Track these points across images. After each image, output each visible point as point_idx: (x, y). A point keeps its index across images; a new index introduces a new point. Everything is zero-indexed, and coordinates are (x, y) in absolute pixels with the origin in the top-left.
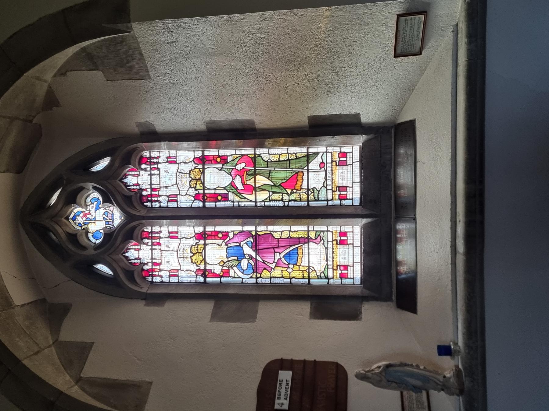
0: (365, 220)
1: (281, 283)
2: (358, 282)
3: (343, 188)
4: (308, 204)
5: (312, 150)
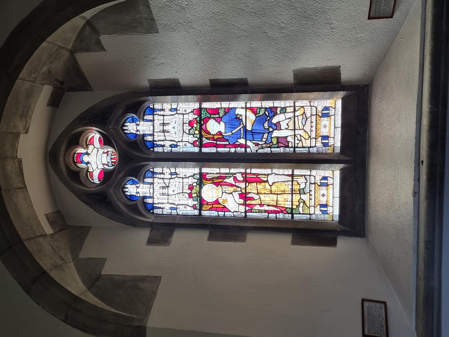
0: (342, 165)
1: (214, 216)
2: (336, 219)
3: (326, 137)
4: (294, 150)
5: (278, 104)
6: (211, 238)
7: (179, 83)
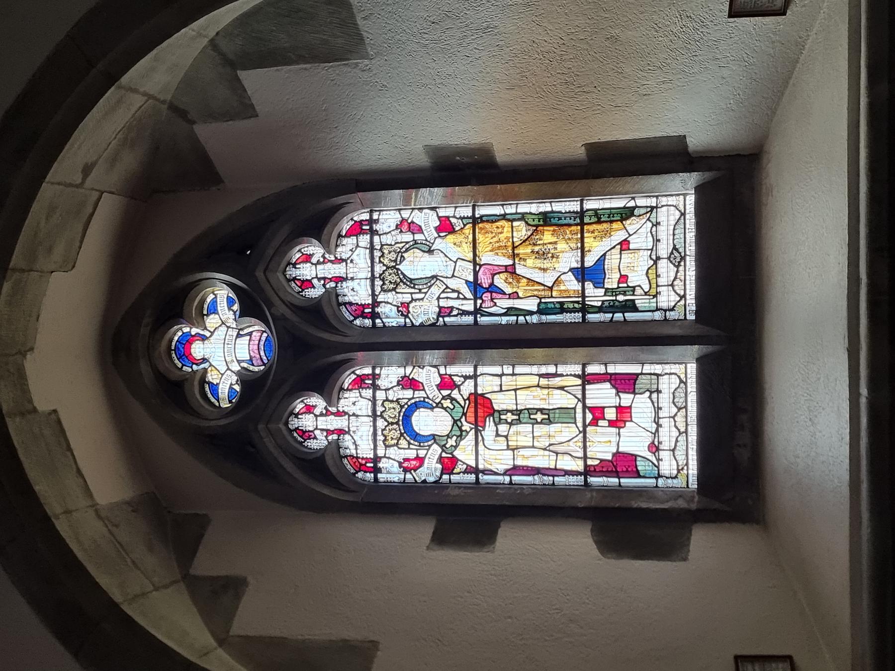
6: (440, 539)
7: (492, 158)
